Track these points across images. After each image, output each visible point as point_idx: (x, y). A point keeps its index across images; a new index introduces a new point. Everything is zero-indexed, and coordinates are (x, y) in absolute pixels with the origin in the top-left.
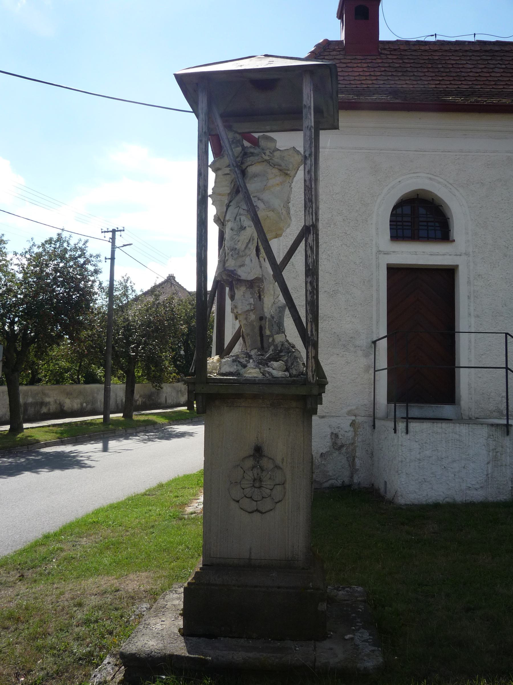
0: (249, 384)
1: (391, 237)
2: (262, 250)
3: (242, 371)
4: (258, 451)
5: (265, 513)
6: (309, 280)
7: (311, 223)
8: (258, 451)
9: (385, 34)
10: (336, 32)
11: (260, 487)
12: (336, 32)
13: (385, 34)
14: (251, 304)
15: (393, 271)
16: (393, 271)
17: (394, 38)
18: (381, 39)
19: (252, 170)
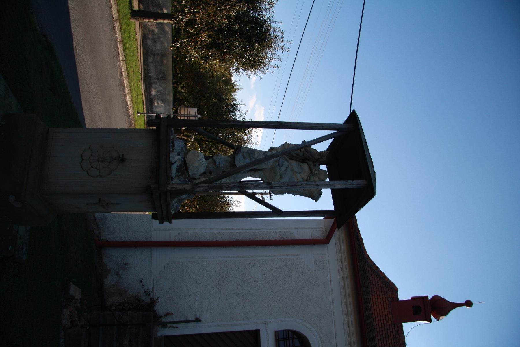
0: (187, 321)
1: (278, 331)
2: (255, 167)
3: (176, 153)
4: (122, 160)
5: (81, 165)
6: (236, 184)
7: (273, 185)
8: (122, 160)
9: (407, 327)
10: (403, 295)
11: (98, 161)
12: (403, 295)
13: (407, 327)
14: (220, 164)
15: (255, 334)
16: (255, 334)
17: (405, 334)
18: (401, 298)
19: (305, 166)
